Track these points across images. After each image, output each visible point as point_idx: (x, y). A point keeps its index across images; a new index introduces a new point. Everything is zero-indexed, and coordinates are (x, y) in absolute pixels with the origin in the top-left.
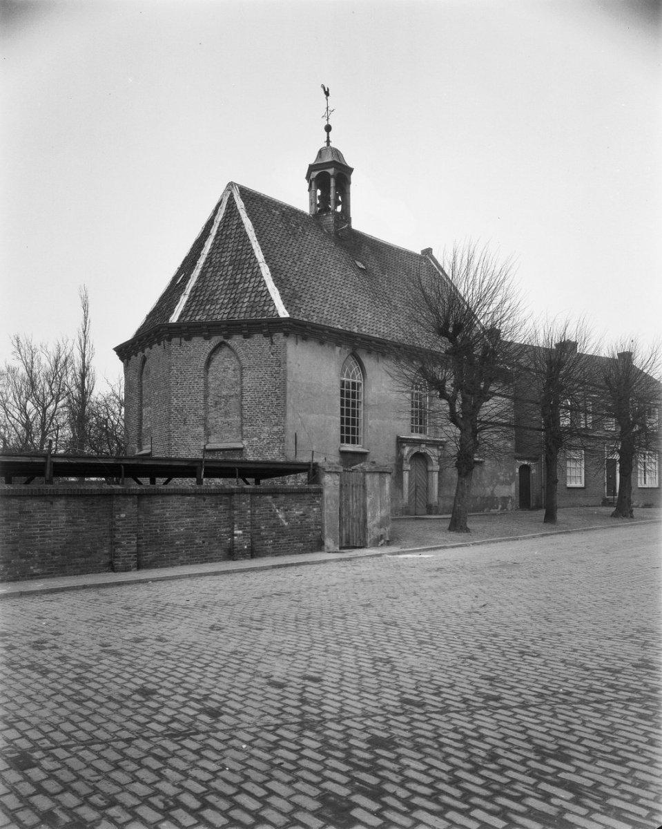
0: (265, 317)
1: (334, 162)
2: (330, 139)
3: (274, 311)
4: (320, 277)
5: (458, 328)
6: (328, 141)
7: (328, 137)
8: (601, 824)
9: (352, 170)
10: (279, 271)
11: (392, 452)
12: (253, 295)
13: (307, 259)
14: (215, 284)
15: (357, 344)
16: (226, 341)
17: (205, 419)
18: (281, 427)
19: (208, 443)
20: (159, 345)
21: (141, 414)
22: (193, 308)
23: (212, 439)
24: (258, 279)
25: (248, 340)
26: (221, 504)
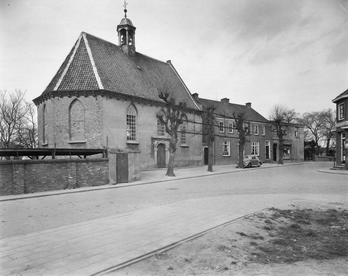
0: (94, 89)
1: (127, 25)
2: (127, 15)
3: (97, 86)
4: (120, 72)
5: (167, 95)
6: (126, 16)
7: (126, 14)
9: (135, 28)
10: (101, 70)
11: (150, 143)
12: (89, 79)
13: (114, 65)
14: (74, 75)
15: (133, 100)
16: (77, 98)
17: (70, 130)
18: (101, 134)
19: (71, 140)
20: (50, 99)
21: (44, 128)
22: (64, 84)
23: (72, 139)
24: (92, 73)
25: (87, 98)
26: (63, 167)
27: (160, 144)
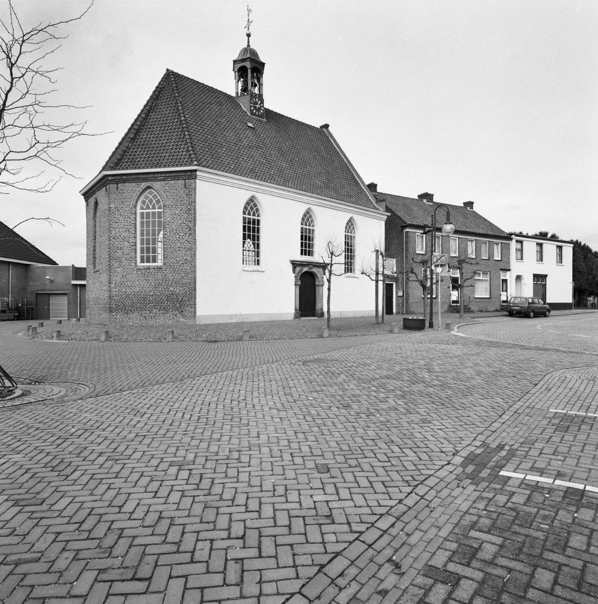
8: (368, 523)
27: (306, 272)
